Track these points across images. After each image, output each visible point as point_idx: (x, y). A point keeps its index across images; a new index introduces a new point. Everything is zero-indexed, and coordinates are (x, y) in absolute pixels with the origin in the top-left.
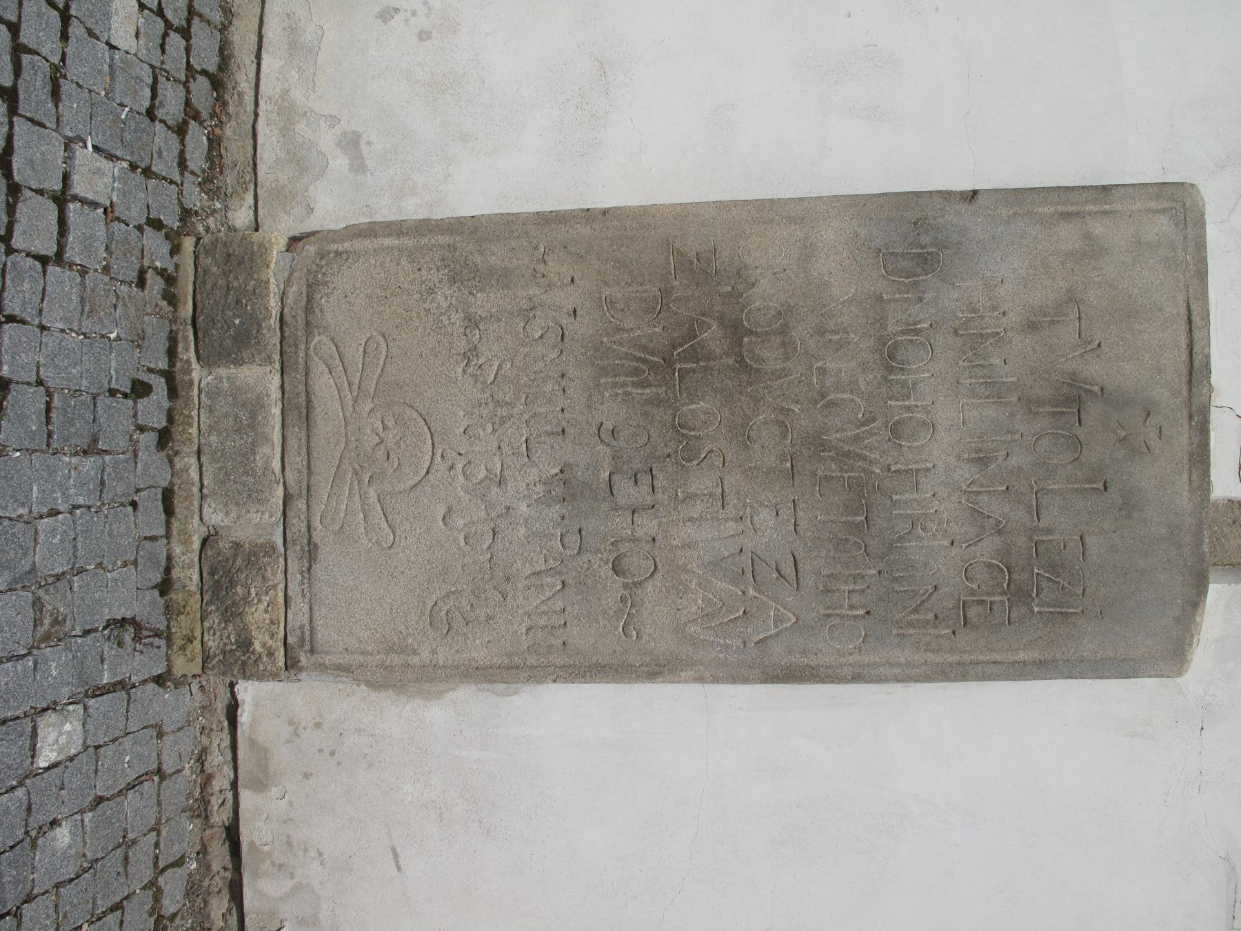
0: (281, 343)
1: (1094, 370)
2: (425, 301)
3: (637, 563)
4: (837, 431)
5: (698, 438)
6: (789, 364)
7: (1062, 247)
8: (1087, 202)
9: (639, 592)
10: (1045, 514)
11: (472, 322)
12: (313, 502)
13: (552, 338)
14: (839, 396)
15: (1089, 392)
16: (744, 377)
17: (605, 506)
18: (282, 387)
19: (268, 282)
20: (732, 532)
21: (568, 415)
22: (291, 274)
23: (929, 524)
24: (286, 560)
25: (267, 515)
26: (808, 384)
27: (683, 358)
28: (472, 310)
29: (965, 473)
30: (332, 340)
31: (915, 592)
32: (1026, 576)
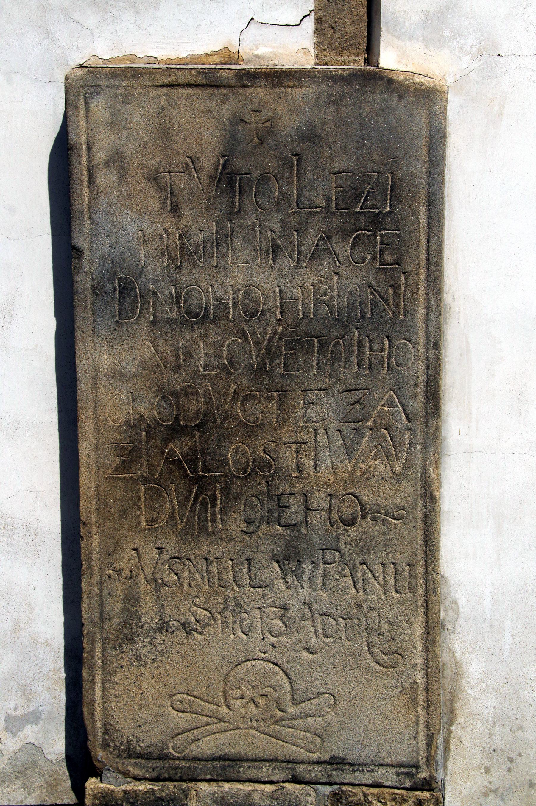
0: (173, 781)
1: (207, 162)
2: (146, 663)
3: (348, 508)
4: (251, 358)
5: (254, 461)
6: (201, 392)
7: (115, 184)
8: (80, 163)
9: (369, 507)
10: (317, 202)
11: (164, 627)
12: (298, 758)
13: (178, 567)
14: (225, 355)
15: (224, 165)
16: (210, 425)
17: (304, 530)
18: (209, 781)
19: (125, 792)
20: (325, 437)
21: (236, 557)
22: (119, 772)
23: (322, 291)
24: (344, 784)
25: (308, 798)
26: (216, 378)
27: (194, 470)
28: (154, 626)
29: (285, 263)
30: (173, 738)
31: (373, 302)
32: (362, 218)
